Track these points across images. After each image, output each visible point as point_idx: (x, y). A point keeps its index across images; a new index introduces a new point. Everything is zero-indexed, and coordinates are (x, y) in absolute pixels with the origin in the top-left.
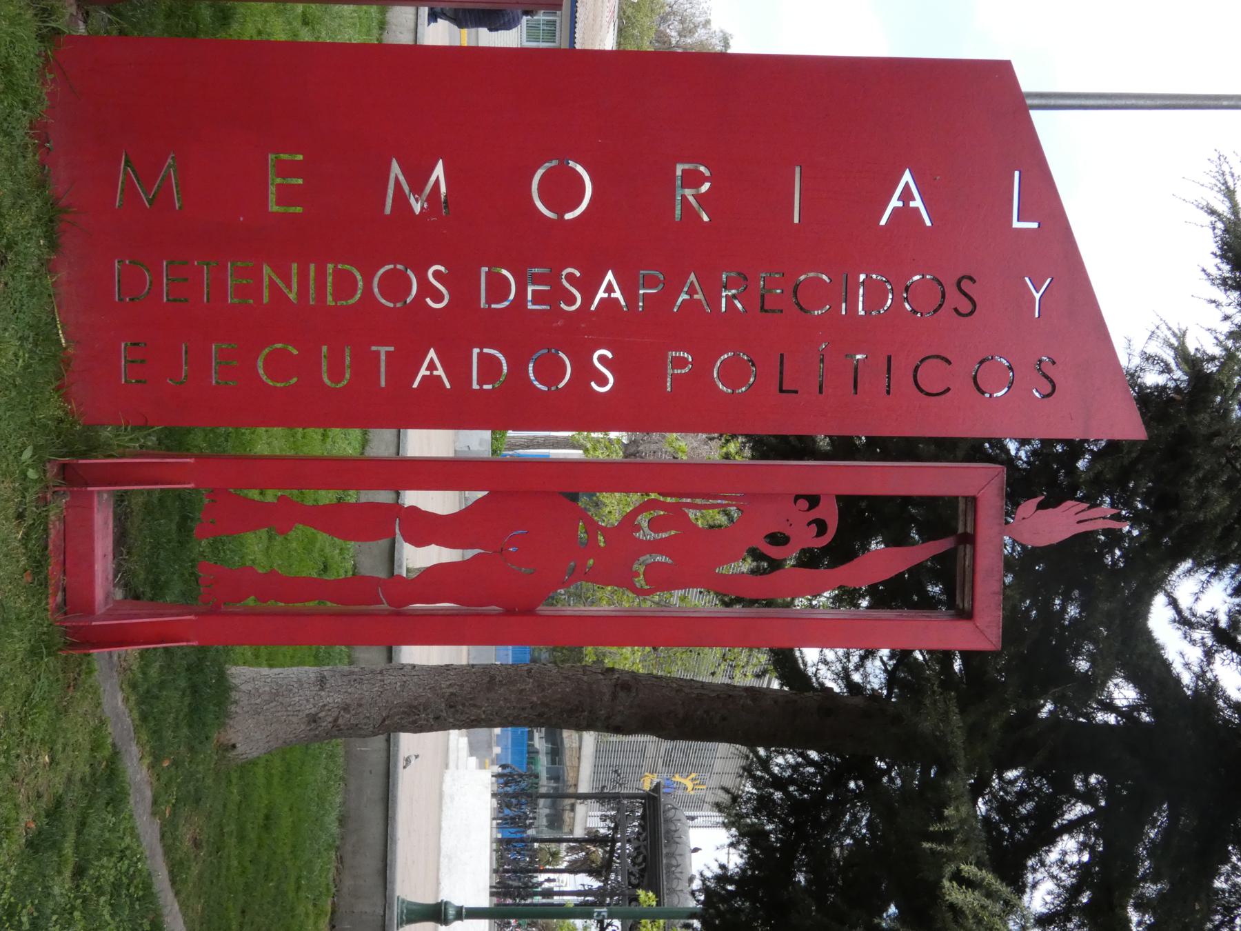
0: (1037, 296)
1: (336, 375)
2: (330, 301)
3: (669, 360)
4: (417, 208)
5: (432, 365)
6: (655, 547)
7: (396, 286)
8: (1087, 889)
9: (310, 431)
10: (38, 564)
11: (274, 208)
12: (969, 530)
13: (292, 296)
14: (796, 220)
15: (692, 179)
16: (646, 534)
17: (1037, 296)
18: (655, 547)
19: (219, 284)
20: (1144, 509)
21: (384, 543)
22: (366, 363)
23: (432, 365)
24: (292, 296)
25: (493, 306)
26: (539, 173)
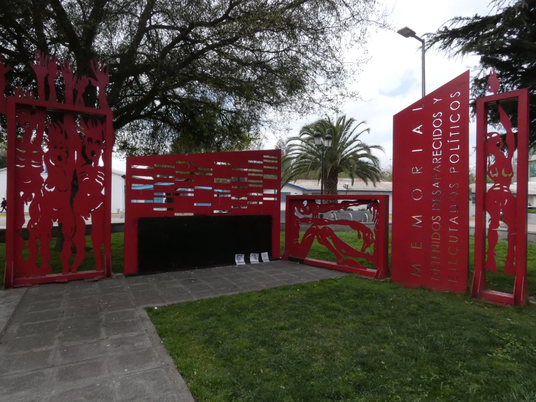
0: (437, 100)
1: (455, 239)
2: (439, 239)
3: (497, 171)
4: (421, 221)
5: (453, 220)
6: (500, 172)
7: (436, 226)
8: (511, 44)
9: (528, 245)
10: (497, 307)
11: (420, 248)
12: (495, 102)
13: (438, 246)
14: (421, 150)
15: (415, 170)
16: (496, 175)
17: (437, 100)
18: (500, 172)
19: (436, 260)
20: (113, 68)
21: (498, 232)
22: (453, 233)
23: (453, 220)
24: (438, 246)
25: (96, 208)
26: (415, 199)
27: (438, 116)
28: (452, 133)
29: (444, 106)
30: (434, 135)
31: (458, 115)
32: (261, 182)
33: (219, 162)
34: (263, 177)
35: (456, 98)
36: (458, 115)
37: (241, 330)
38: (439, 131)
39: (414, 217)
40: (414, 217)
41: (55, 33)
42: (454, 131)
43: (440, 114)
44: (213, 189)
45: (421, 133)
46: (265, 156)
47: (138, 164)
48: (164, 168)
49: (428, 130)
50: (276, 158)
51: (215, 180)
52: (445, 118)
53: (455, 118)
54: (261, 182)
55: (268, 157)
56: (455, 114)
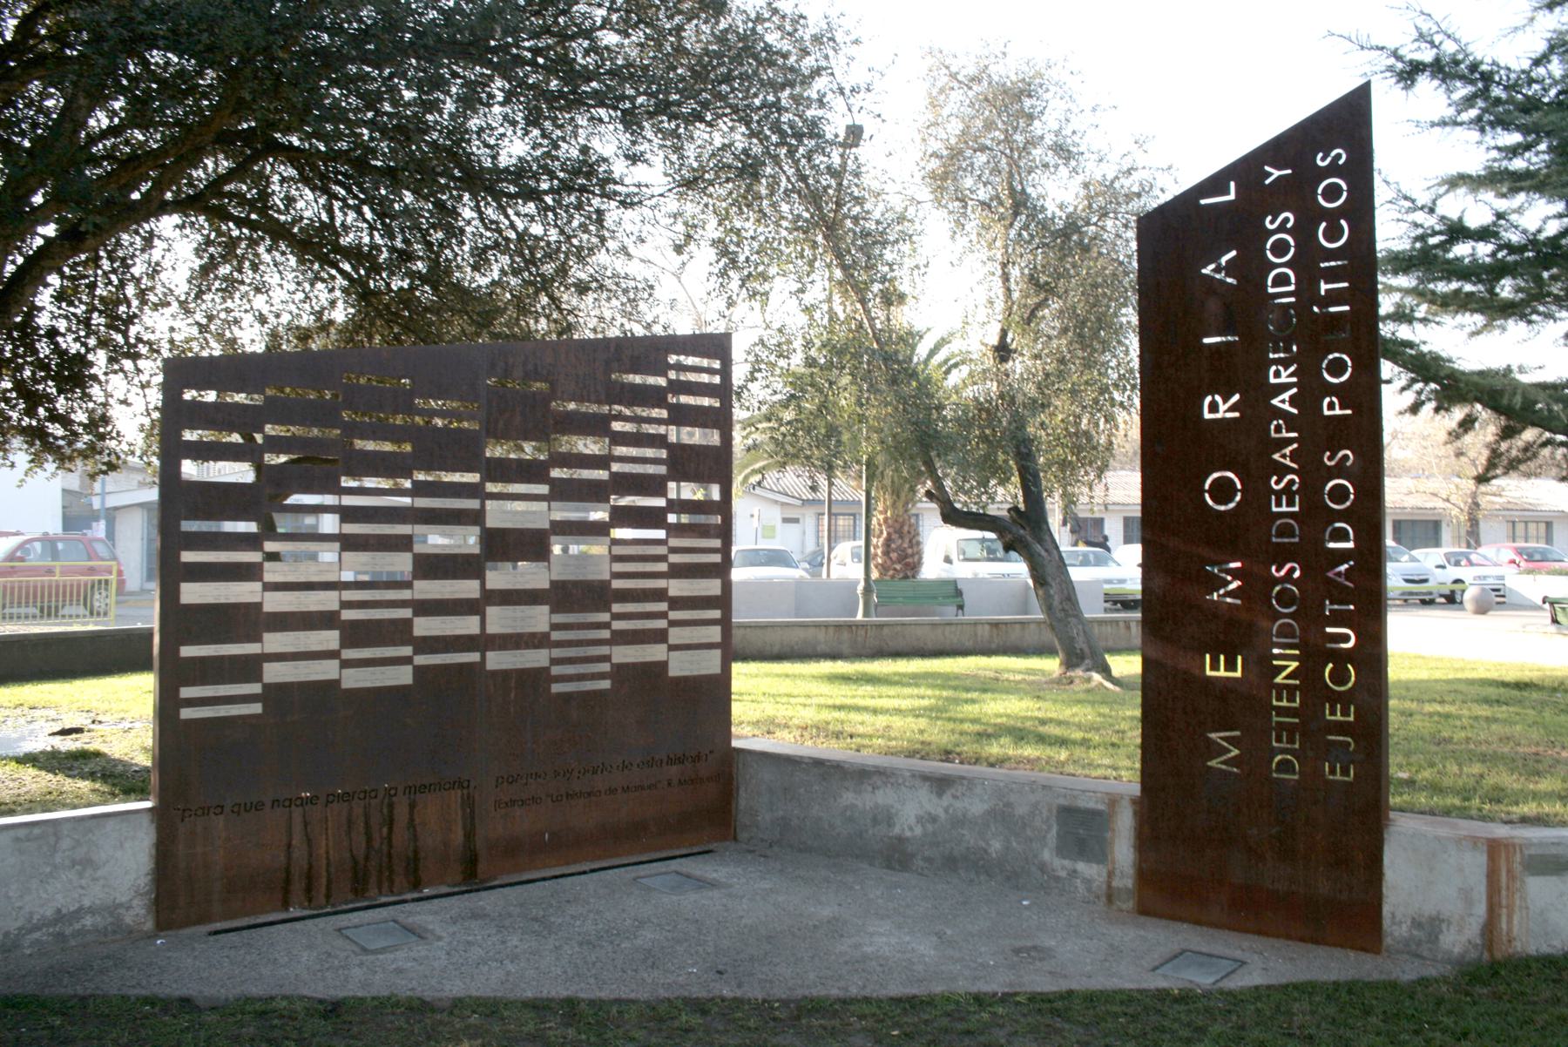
0: (1276, 173)
17: (1276, 173)
27: (1279, 224)
28: (1326, 283)
29: (1297, 192)
30: (1273, 286)
31: (1343, 222)
32: (663, 454)
33: (193, 428)
34: (343, 520)
35: (1333, 169)
36: (1343, 222)
37: (834, 741)
38: (1286, 276)
39: (1213, 736)
40: (1213, 736)
41: (472, 69)
42: (1331, 275)
43: (1286, 220)
44: (485, 479)
45: (1295, 411)
46: (672, 359)
47: (1338, 266)
48: (1335, 260)
49: (1252, 268)
50: (717, 365)
51: (495, 451)
52: (1304, 232)
53: (1334, 234)
54: (663, 454)
55: (207, 435)
56: (1332, 217)
